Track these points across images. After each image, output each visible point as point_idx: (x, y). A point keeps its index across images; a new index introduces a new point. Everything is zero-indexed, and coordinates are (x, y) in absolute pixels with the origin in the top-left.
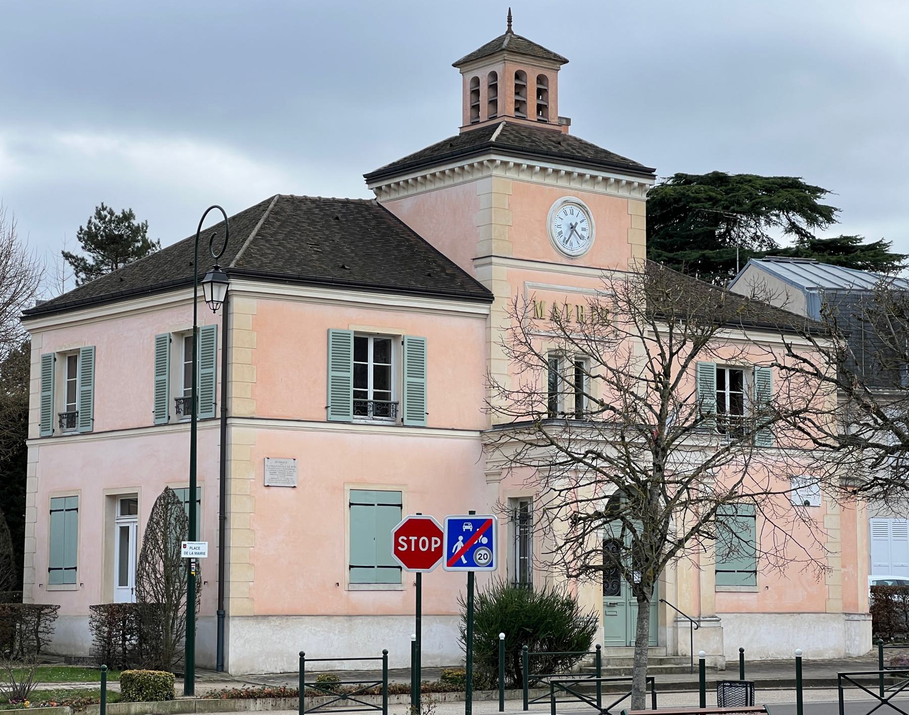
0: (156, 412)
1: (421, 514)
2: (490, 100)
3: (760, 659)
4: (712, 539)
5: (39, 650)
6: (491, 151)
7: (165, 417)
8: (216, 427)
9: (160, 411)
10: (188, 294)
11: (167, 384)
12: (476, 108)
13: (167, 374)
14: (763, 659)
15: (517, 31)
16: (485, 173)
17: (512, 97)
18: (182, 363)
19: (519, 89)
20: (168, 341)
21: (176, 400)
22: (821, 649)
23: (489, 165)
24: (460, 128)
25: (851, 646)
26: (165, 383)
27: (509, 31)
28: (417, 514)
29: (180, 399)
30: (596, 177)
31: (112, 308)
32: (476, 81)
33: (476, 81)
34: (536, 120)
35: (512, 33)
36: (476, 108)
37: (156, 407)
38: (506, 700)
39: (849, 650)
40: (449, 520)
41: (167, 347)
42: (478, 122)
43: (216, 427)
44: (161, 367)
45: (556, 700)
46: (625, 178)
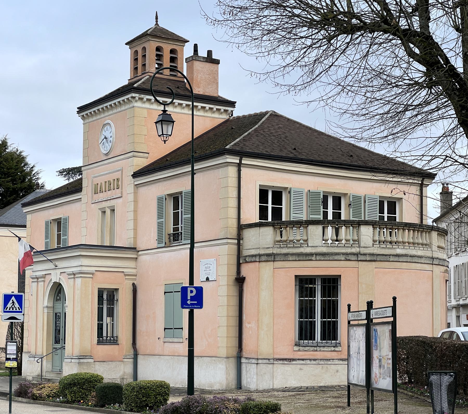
0: (158, 240)
1: (14, 292)
3: (181, 387)
6: (132, 92)
9: (160, 240)
10: (188, 168)
11: (68, 220)
12: (136, 69)
14: (183, 387)
15: (162, 24)
16: (131, 105)
18: (56, 233)
19: (159, 57)
20: (164, 199)
21: (169, 234)
22: (213, 382)
24: (129, 80)
25: (250, 383)
26: (163, 223)
27: (157, 24)
28: (12, 292)
29: (171, 234)
30: (204, 107)
31: (151, 177)
32: (136, 52)
33: (136, 52)
36: (136, 69)
37: (158, 237)
39: (249, 386)
40: (4, 295)
42: (137, 76)
44: (160, 215)
46: (215, 107)
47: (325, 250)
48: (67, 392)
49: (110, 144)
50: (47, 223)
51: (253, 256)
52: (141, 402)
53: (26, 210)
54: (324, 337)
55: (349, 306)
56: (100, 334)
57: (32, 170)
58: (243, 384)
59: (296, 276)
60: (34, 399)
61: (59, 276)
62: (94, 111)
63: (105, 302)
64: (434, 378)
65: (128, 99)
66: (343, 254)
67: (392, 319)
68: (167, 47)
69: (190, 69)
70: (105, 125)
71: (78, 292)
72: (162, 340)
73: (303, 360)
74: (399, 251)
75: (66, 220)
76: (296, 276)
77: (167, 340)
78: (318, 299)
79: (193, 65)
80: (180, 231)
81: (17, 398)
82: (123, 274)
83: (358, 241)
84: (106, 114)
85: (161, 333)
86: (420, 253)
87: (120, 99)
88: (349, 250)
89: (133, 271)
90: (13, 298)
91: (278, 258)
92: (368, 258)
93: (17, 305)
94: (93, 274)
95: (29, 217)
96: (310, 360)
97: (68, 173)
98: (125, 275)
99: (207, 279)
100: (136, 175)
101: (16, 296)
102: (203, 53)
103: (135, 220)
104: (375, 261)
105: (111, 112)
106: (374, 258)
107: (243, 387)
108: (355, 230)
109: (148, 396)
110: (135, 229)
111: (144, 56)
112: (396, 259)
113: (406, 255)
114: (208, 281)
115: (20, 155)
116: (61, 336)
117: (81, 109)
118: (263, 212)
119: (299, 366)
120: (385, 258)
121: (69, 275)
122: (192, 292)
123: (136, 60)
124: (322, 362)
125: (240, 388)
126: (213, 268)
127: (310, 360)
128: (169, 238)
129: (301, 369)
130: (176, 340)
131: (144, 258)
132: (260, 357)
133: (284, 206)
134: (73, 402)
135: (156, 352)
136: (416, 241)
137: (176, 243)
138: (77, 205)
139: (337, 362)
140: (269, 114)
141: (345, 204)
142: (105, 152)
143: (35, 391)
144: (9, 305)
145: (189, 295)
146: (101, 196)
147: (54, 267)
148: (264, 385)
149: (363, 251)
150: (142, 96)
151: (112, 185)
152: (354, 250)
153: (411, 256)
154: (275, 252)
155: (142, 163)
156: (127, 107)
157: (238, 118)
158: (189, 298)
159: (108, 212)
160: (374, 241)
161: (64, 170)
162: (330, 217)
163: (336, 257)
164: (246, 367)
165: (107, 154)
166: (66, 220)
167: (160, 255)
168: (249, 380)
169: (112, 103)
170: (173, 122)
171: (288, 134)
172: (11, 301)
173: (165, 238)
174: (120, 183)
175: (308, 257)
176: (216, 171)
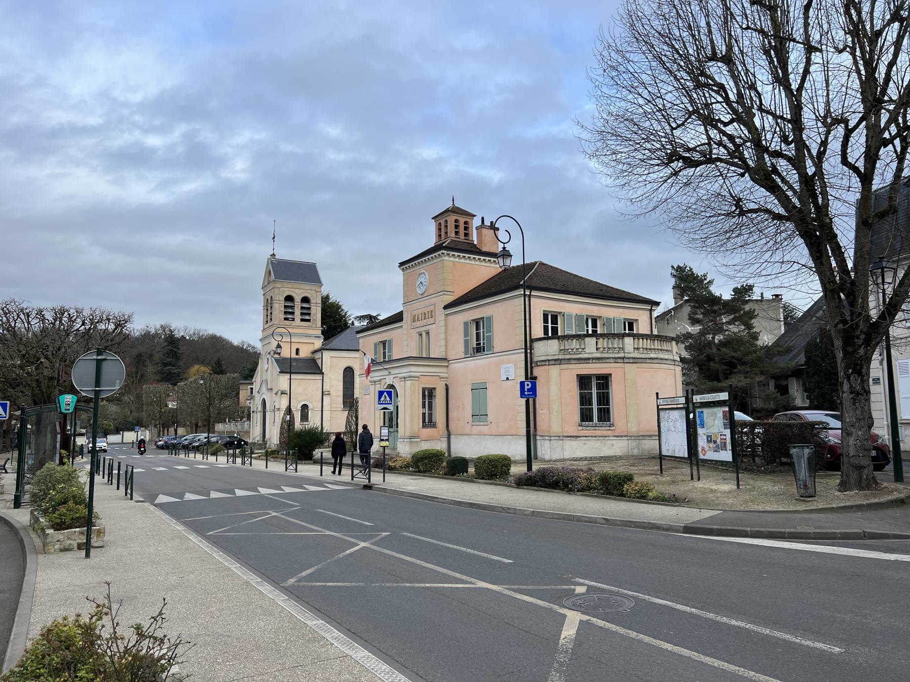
4: (522, 395)
5: (365, 455)
8: (522, 353)
9: (466, 352)
12: (440, 235)
15: (457, 205)
16: (441, 259)
17: (454, 230)
18: (475, 332)
19: (456, 227)
27: (453, 204)
32: (440, 224)
33: (440, 224)
36: (440, 235)
43: (522, 353)
44: (466, 334)
45: (840, 431)
47: (598, 355)
48: (420, 464)
49: (425, 287)
50: (375, 344)
51: (543, 361)
52: (491, 472)
53: (359, 336)
54: (600, 420)
55: (657, 394)
56: (424, 421)
57: (346, 314)
58: (538, 456)
59: (577, 375)
60: (389, 470)
61: (392, 380)
62: (412, 265)
63: (427, 397)
64: (793, 451)
65: (439, 255)
66: (613, 358)
67: (686, 405)
68: (462, 220)
69: (479, 235)
70: (420, 274)
71: (408, 391)
72: (470, 423)
73: (586, 437)
74: (652, 355)
75: (390, 341)
76: (577, 375)
77: (474, 423)
78: (594, 391)
79: (481, 231)
80: (482, 345)
81: (374, 469)
82: (438, 377)
83: (623, 349)
84: (421, 266)
85: (470, 419)
86: (666, 357)
87: (433, 255)
88: (617, 355)
89: (446, 375)
90: (385, 393)
91: (563, 362)
92: (631, 361)
93: (388, 399)
94: (418, 377)
95: (361, 341)
96: (592, 437)
97: (360, 319)
98: (441, 378)
99: (507, 379)
100: (446, 307)
101: (387, 392)
102: (487, 223)
103: (446, 339)
104: (636, 363)
105: (425, 265)
106: (636, 361)
107: (538, 458)
108: (621, 340)
109: (496, 467)
110: (446, 345)
111: (446, 226)
112: (651, 361)
113: (657, 358)
115: (338, 304)
116: (394, 423)
117: (402, 264)
118: (546, 329)
119: (583, 442)
120: (643, 360)
121: (400, 378)
122: (528, 385)
123: (440, 229)
124: (601, 439)
125: (537, 459)
126: (512, 370)
127: (592, 437)
128: (474, 351)
129: (585, 444)
130: (482, 423)
131: (456, 366)
132: (552, 435)
133: (559, 326)
134: (425, 472)
135: (466, 433)
136: (663, 348)
137: (479, 354)
138: (399, 331)
139: (612, 438)
140: (537, 264)
141: (600, 324)
142: (421, 293)
143: (391, 464)
144: (382, 399)
145: (526, 387)
146: (418, 324)
147: (388, 374)
148: (556, 456)
149: (627, 355)
150: (449, 252)
151: (427, 316)
152: (621, 355)
153: (660, 359)
154: (560, 358)
155: (450, 299)
156: (438, 260)
157: (513, 267)
158: (526, 390)
159: (424, 334)
160: (634, 349)
161: (358, 317)
162: (590, 332)
163: (608, 361)
164: (541, 443)
165: (422, 294)
166: (390, 341)
167: (467, 363)
168: (543, 452)
169: (426, 258)
170: (511, 256)
171: (554, 276)
172: (384, 396)
173: (471, 351)
174: (433, 314)
175: (581, 360)
176: (480, 308)
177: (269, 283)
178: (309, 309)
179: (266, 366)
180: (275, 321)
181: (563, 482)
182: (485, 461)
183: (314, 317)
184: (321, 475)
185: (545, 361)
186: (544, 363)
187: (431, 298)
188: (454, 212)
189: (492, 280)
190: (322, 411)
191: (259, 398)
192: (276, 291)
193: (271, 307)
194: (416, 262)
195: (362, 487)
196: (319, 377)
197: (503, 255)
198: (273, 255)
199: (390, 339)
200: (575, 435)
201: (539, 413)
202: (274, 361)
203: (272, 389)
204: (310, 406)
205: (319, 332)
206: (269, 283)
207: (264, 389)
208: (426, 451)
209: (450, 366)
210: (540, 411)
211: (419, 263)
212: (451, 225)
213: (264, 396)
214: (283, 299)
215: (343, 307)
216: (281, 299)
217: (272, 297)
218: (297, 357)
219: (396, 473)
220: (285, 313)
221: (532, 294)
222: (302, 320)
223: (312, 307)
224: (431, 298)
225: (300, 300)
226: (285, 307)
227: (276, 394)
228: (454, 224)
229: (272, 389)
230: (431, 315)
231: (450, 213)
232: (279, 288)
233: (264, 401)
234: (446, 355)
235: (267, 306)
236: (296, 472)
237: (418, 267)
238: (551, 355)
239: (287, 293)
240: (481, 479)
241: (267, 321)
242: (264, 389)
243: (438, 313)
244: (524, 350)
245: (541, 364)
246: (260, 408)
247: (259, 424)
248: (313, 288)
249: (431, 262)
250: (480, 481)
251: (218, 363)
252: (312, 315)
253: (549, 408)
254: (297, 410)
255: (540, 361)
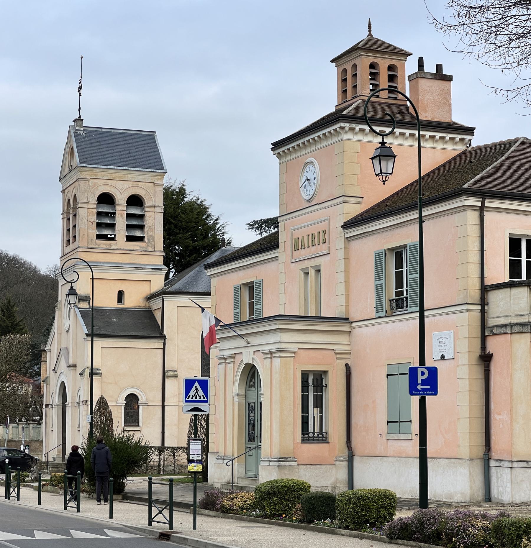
0: (377, 308)
1: (197, 377)
2: (353, 85)
6: (341, 121)
7: (383, 311)
12: (345, 92)
13: (384, 279)
15: (376, 35)
16: (340, 138)
18: (393, 271)
19: (374, 76)
20: (384, 255)
23: (341, 131)
24: (336, 106)
27: (370, 35)
28: (195, 376)
29: (393, 300)
32: (345, 71)
33: (345, 71)
34: (387, 97)
35: (372, 36)
36: (345, 92)
38: (42, 491)
39: (501, 497)
41: (384, 259)
42: (347, 101)
48: (265, 503)
49: (314, 187)
50: (236, 289)
51: (502, 326)
52: (359, 517)
57: (216, 223)
61: (252, 356)
63: (311, 389)
65: (335, 130)
68: (383, 63)
70: (306, 164)
72: (384, 437)
75: (259, 284)
77: (391, 436)
79: (417, 82)
81: (202, 511)
82: (333, 352)
84: (308, 150)
85: (383, 427)
89: (346, 348)
90: (197, 384)
93: (201, 393)
94: (294, 352)
95: (214, 281)
98: (336, 354)
99: (443, 357)
100: (347, 226)
101: (200, 382)
102: (430, 68)
103: (347, 283)
105: (314, 148)
109: (368, 509)
110: (347, 295)
111: (355, 75)
114: (444, 359)
117: (277, 145)
121: (264, 354)
122: (423, 374)
123: (345, 80)
125: (490, 500)
126: (450, 342)
128: (391, 305)
130: (402, 437)
134: (273, 516)
135: (377, 453)
138: (272, 266)
140: (519, 142)
142: (308, 198)
143: (225, 502)
144: (192, 393)
145: (420, 378)
146: (303, 253)
147: (245, 344)
150: (354, 126)
156: (335, 139)
157: (479, 148)
158: (419, 382)
159: (312, 273)
161: (256, 223)
164: (497, 473)
165: (309, 200)
166: (259, 284)
167: (379, 326)
170: (395, 157)
172: (194, 388)
173: (386, 305)
174: (326, 236)
177: (70, 171)
178: (142, 217)
179: (66, 323)
180: (80, 242)
181: (446, 532)
182: (350, 499)
183: (150, 233)
184: (111, 517)
185: (505, 326)
186: (503, 330)
187: (312, 212)
188: (369, 50)
189: (443, 171)
190: (163, 406)
191: (55, 381)
192: (82, 183)
193: (75, 215)
194: (300, 142)
195: (158, 535)
196: (157, 344)
197: (379, 156)
198: (79, 120)
199: (259, 279)
200: (436, 456)
201: (494, 418)
202: (79, 314)
203: (75, 366)
204: (142, 399)
205: (159, 261)
206: (70, 171)
207: (63, 364)
208: (276, 482)
209: (356, 332)
210: (496, 416)
211: (303, 143)
212: (364, 73)
213: (63, 378)
214: (94, 199)
215: (211, 211)
216: (91, 201)
217: (75, 196)
218: (120, 306)
219: (232, 518)
220: (99, 225)
221: (486, 204)
222: (129, 238)
223: (147, 214)
224: (312, 212)
225: (124, 202)
226: (99, 214)
227: (81, 374)
228: (369, 70)
229: (75, 366)
230: (324, 239)
231: (360, 52)
232: (87, 180)
233: (63, 384)
234: (347, 311)
235: (68, 213)
236: (79, 511)
237: (303, 152)
238: (517, 315)
239: (103, 189)
240: (345, 528)
241: (69, 241)
242: (63, 364)
243: (333, 236)
244: (418, 314)
245: (498, 332)
246: (57, 400)
247: (55, 429)
248: (149, 178)
249: (324, 144)
250: (343, 531)
251: (8, 309)
252: (146, 229)
253: (511, 410)
254: (118, 405)
255: (497, 326)
